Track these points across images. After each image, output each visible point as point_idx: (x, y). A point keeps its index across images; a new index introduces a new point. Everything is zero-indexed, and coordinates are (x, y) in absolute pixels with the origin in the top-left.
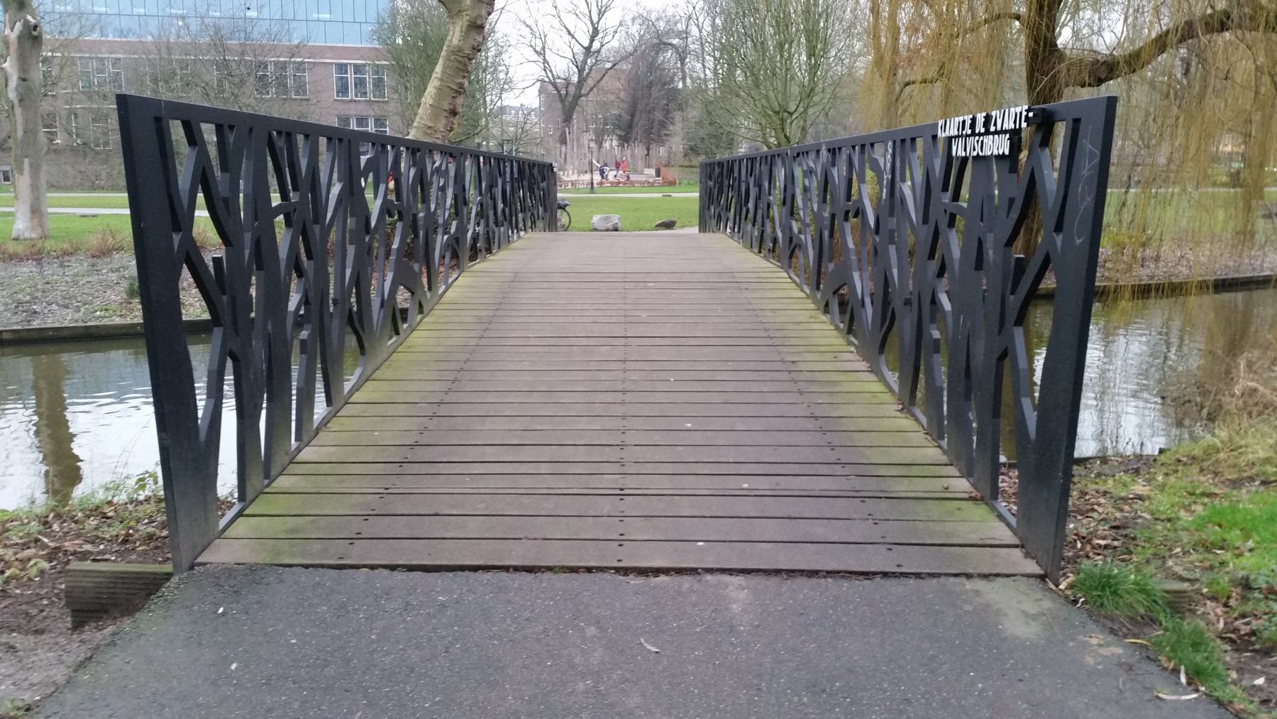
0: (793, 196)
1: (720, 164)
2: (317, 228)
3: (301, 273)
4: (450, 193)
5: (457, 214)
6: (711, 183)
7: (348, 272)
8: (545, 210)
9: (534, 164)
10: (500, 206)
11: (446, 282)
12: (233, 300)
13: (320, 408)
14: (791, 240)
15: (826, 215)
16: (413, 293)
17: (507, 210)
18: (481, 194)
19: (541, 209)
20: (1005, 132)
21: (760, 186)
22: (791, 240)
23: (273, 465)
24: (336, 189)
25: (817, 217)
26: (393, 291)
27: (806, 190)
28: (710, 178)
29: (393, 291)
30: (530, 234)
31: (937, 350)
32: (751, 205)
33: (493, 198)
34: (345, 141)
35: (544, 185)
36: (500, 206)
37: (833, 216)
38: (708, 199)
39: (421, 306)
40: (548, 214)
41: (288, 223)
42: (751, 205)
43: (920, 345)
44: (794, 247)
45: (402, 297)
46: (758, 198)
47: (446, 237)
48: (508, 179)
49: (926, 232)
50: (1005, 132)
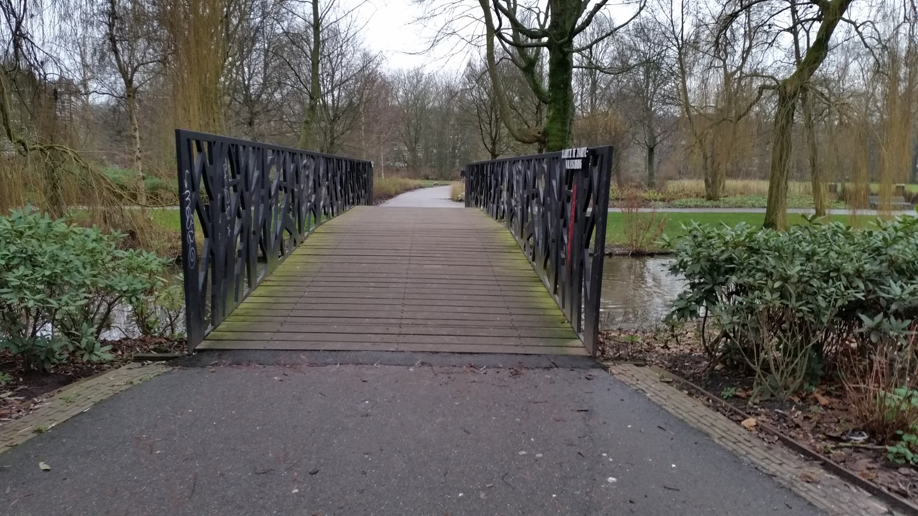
0: (513, 185)
1: (477, 166)
2: (247, 193)
3: (239, 216)
4: (311, 178)
5: (315, 192)
6: (472, 178)
7: (260, 218)
8: (366, 192)
9: (360, 163)
10: (339, 188)
11: (308, 230)
12: (213, 226)
13: (246, 291)
14: (511, 210)
15: (525, 196)
16: (291, 234)
17: (343, 191)
18: (327, 180)
19: (363, 191)
20: (579, 158)
21: (497, 180)
22: (511, 210)
23: (226, 310)
24: (256, 174)
25: (522, 196)
26: (281, 232)
27: (518, 182)
28: (472, 175)
29: (281, 232)
30: (357, 207)
31: (563, 264)
32: (492, 191)
33: (335, 183)
34: (261, 150)
35: (365, 176)
36: (339, 188)
37: (528, 196)
38: (470, 189)
39: (295, 242)
40: (367, 194)
41: (235, 190)
42: (492, 191)
43: (558, 262)
44: (512, 214)
45: (286, 236)
46: (496, 186)
47: (309, 204)
48: (344, 172)
49: (560, 203)
50: (579, 158)
